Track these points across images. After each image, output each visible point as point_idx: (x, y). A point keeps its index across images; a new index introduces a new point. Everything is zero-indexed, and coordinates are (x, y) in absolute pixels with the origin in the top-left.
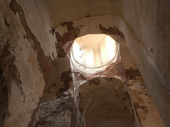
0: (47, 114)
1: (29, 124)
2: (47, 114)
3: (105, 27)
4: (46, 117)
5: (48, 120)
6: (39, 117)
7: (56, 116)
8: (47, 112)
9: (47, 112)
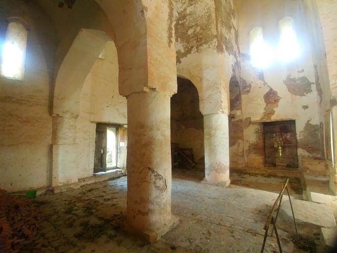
0: (185, 6)
1: (169, 15)
2: (185, 6)
3: (120, 96)
4: (185, 10)
5: (188, 12)
6: (178, 12)
7: (195, 4)
8: (184, 3)
9: (184, 3)
